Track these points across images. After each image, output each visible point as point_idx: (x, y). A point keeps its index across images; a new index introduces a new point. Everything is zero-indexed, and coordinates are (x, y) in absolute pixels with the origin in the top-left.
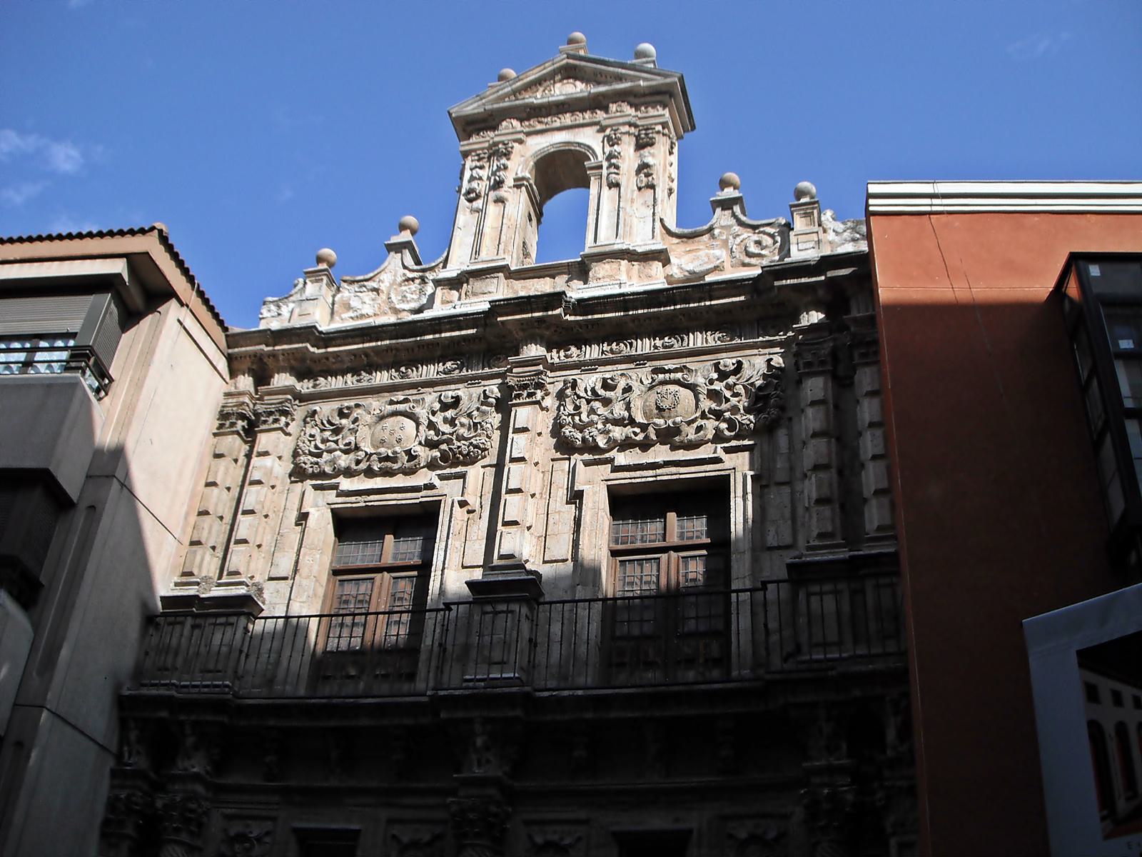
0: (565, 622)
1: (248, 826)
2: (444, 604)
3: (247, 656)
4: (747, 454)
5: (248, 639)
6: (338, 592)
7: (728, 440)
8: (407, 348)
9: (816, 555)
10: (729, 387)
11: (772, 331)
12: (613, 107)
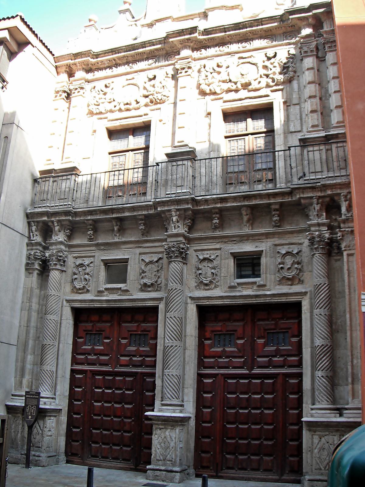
0: (207, 167)
1: (84, 260)
2: (156, 163)
3: (77, 191)
4: (281, 92)
5: (76, 184)
6: (112, 161)
7: (272, 87)
8: (132, 56)
9: (311, 134)
10: (272, 64)
11: (289, 38)
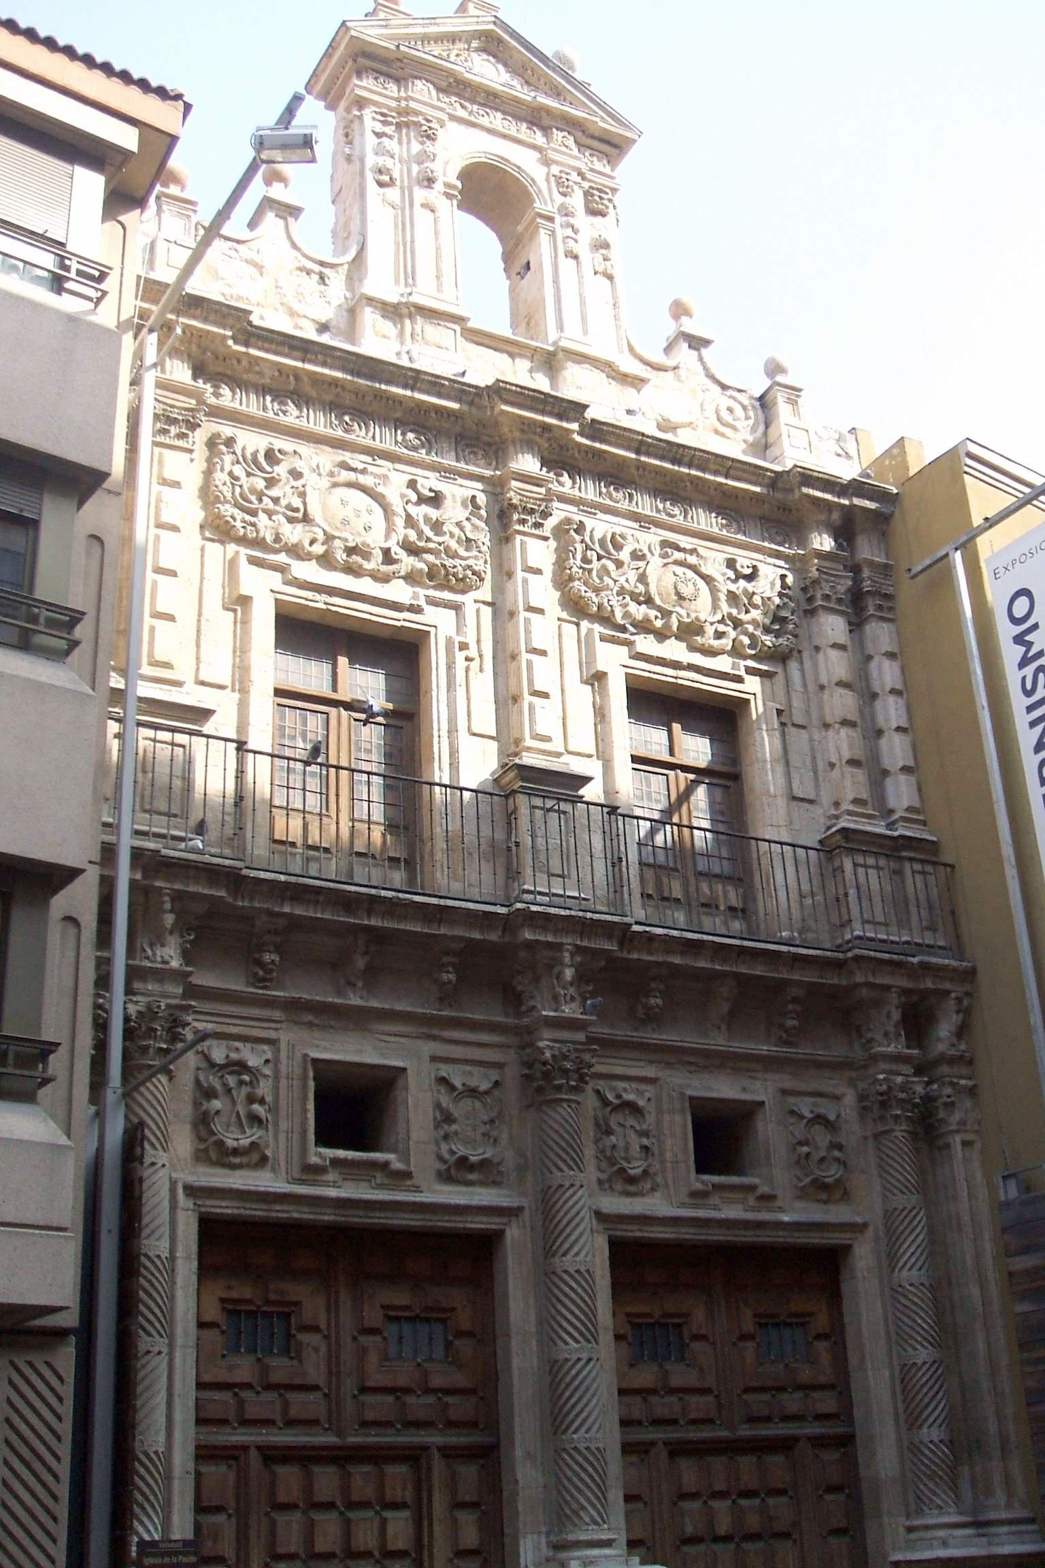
7: (745, 657)
8: (358, 393)
12: (558, 135)
